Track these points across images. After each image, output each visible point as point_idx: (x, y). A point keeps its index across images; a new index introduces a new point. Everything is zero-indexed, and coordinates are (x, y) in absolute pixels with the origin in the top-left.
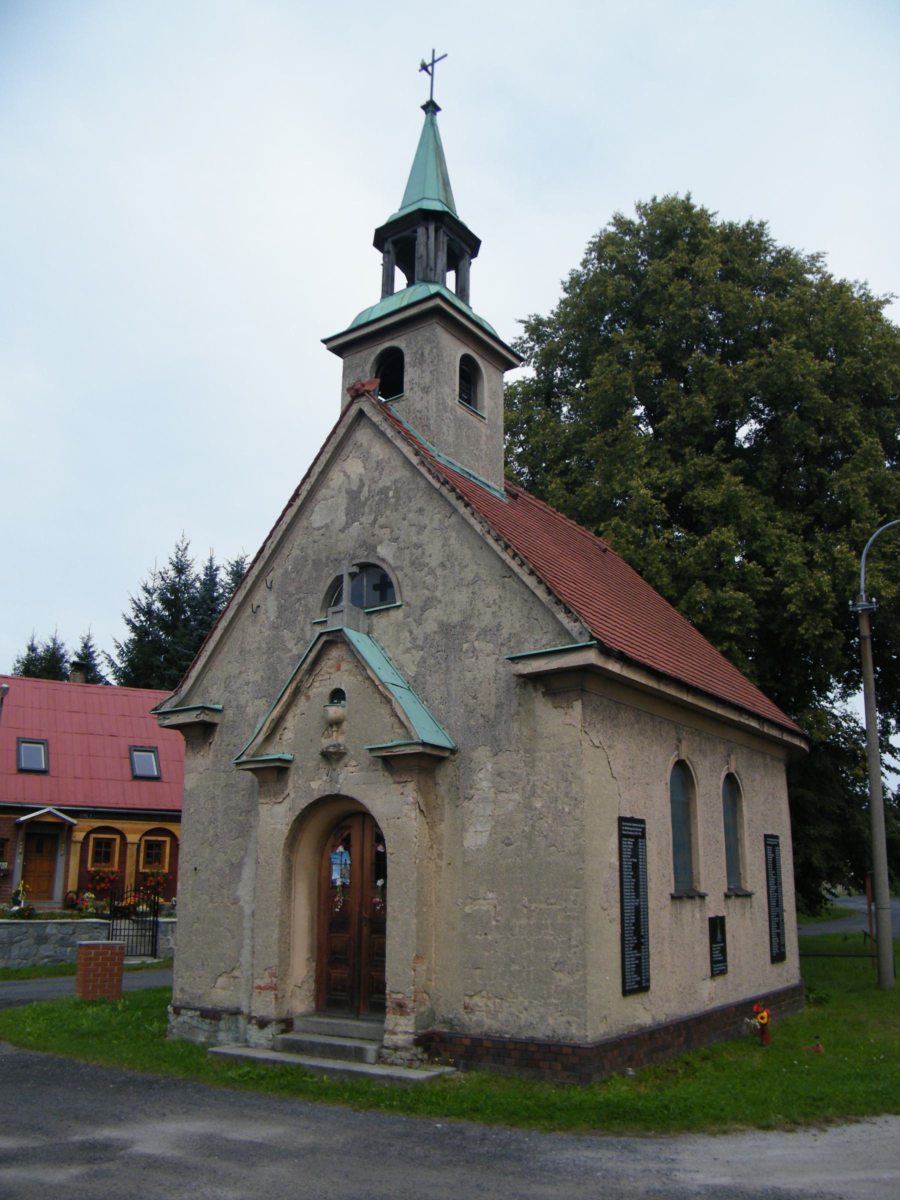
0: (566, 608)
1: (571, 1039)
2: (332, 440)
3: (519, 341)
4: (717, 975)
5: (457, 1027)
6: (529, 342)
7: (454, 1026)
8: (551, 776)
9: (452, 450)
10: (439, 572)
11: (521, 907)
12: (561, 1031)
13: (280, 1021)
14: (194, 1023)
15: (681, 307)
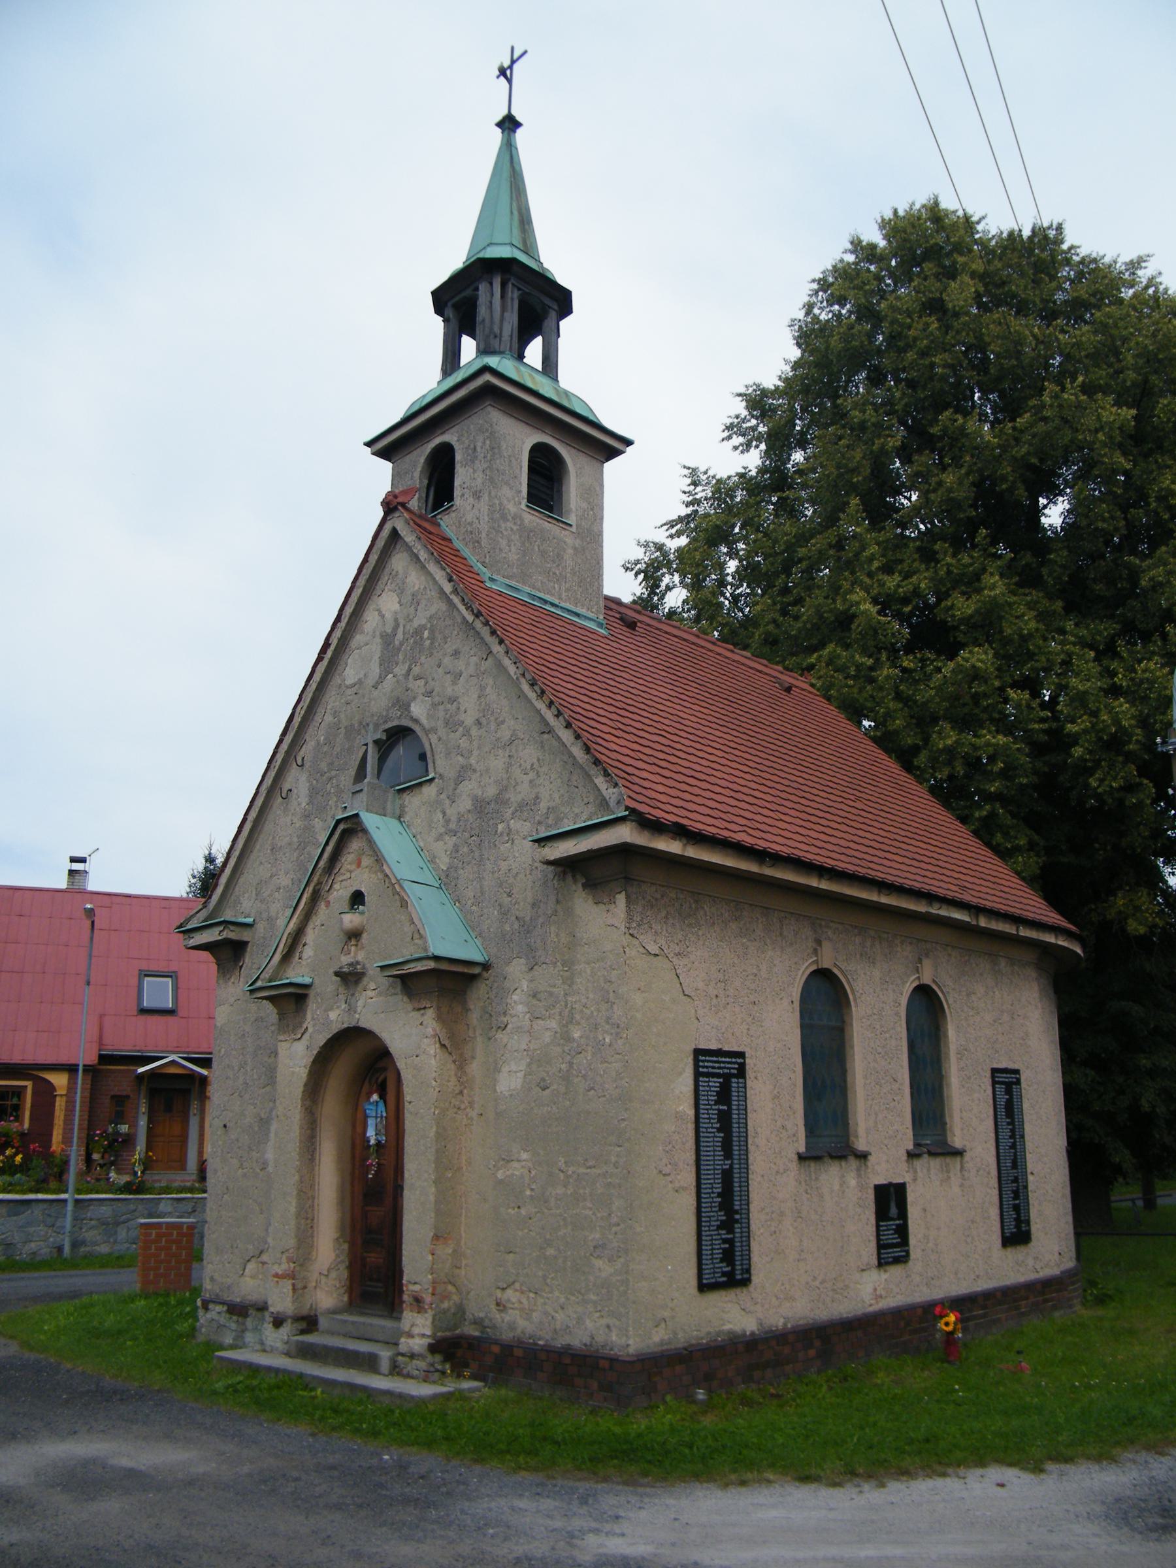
0: (605, 770)
1: (611, 1349)
2: (364, 571)
3: (736, 421)
4: (888, 1263)
5: (488, 1330)
6: (749, 421)
7: (485, 1327)
8: (591, 996)
9: (515, 570)
10: (474, 732)
11: (557, 1171)
12: (600, 1339)
13: (298, 1319)
14: (222, 1320)
15: (923, 354)
